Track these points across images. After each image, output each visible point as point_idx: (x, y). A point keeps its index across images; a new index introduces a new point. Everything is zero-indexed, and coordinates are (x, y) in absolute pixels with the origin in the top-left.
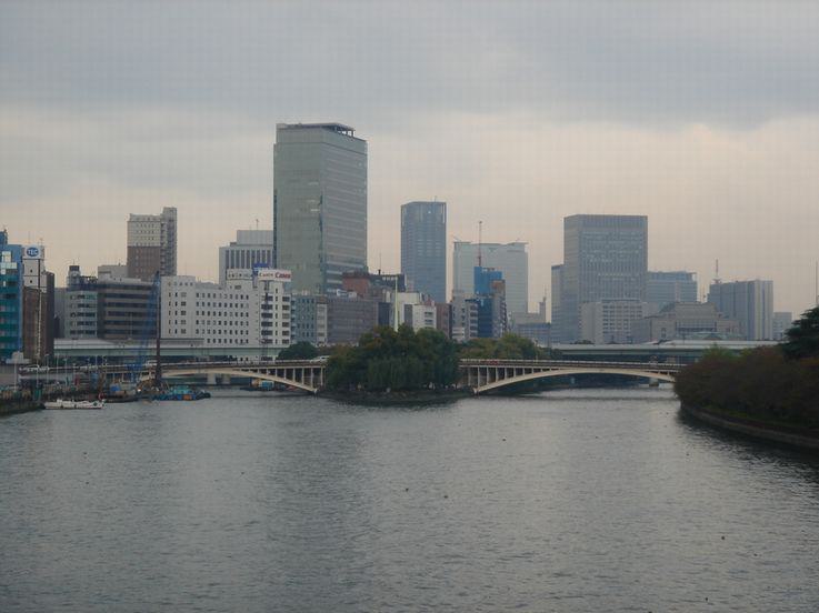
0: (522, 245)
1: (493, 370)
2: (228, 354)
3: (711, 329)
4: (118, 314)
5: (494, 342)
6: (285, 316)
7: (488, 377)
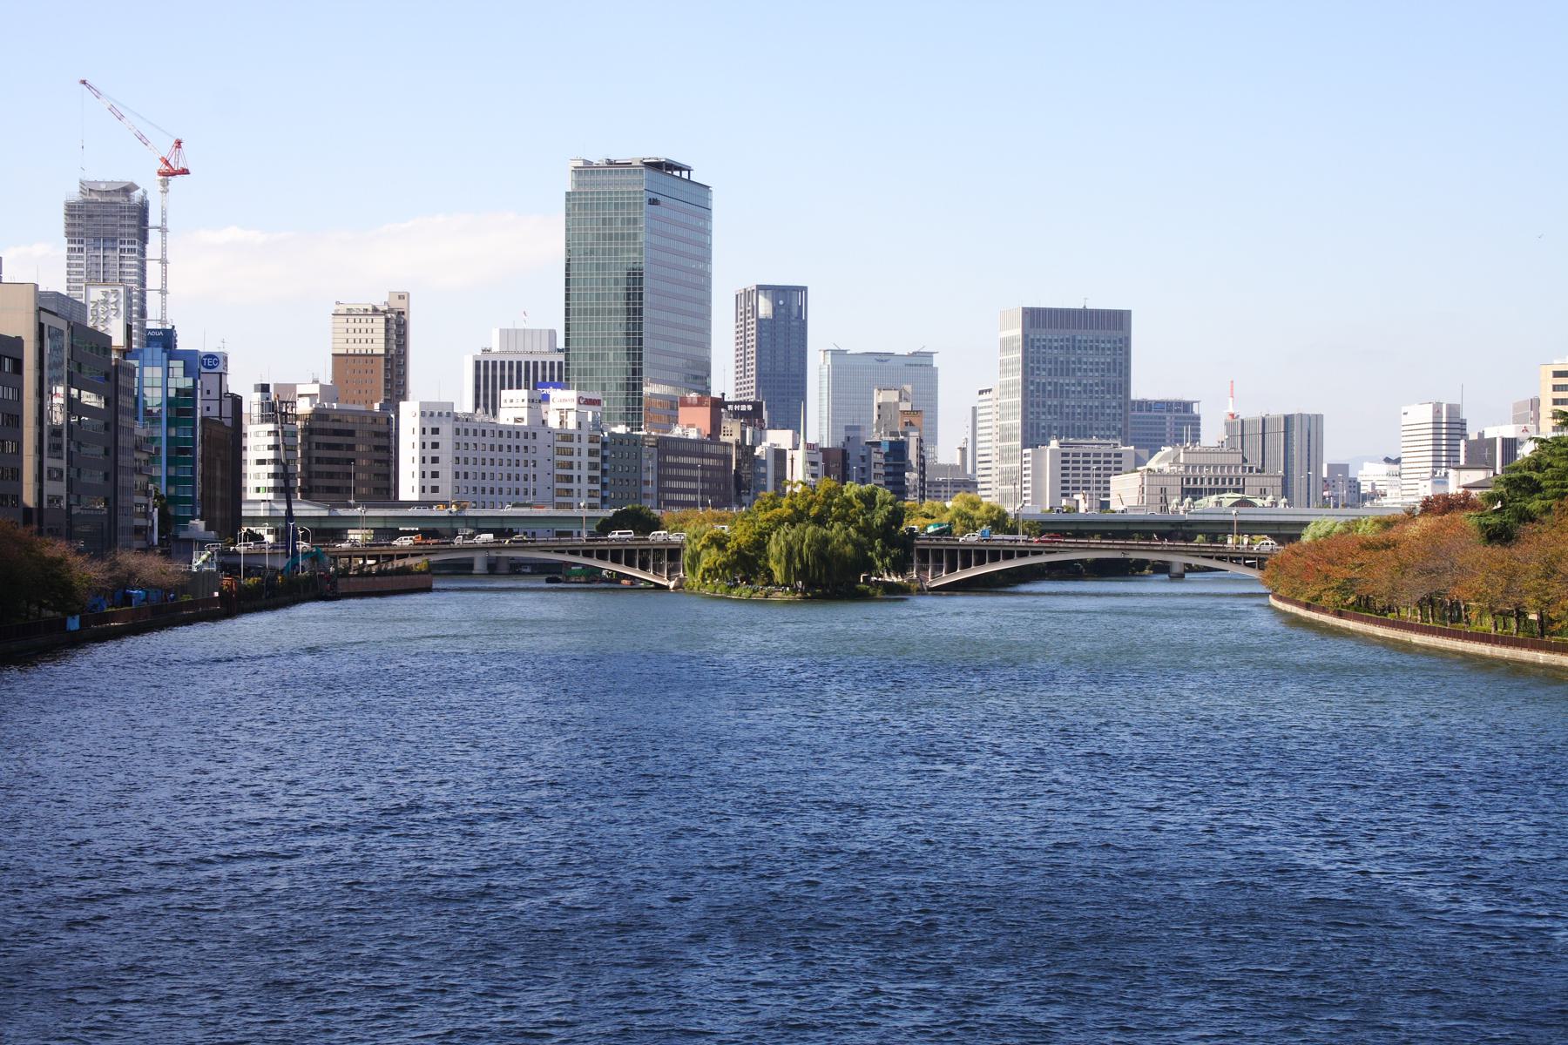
0: (930, 355)
2: (507, 526)
3: (1237, 491)
4: (331, 461)
5: (1508, 492)
6: (593, 466)
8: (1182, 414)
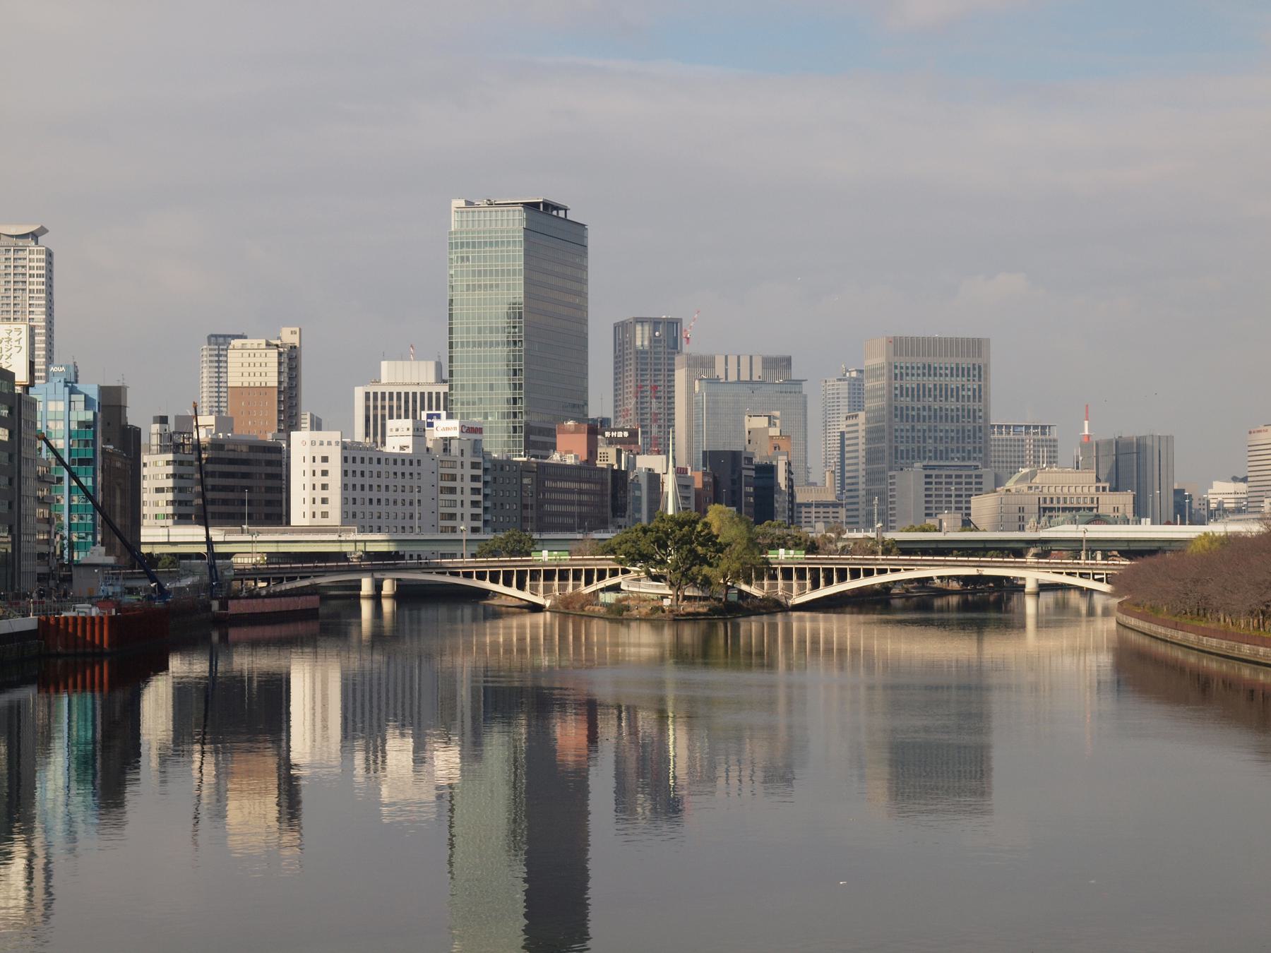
1: (815, 572)
7: (808, 582)
8: (1040, 437)
